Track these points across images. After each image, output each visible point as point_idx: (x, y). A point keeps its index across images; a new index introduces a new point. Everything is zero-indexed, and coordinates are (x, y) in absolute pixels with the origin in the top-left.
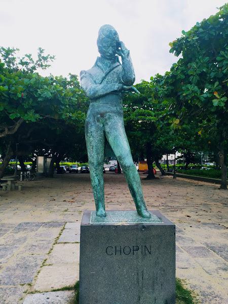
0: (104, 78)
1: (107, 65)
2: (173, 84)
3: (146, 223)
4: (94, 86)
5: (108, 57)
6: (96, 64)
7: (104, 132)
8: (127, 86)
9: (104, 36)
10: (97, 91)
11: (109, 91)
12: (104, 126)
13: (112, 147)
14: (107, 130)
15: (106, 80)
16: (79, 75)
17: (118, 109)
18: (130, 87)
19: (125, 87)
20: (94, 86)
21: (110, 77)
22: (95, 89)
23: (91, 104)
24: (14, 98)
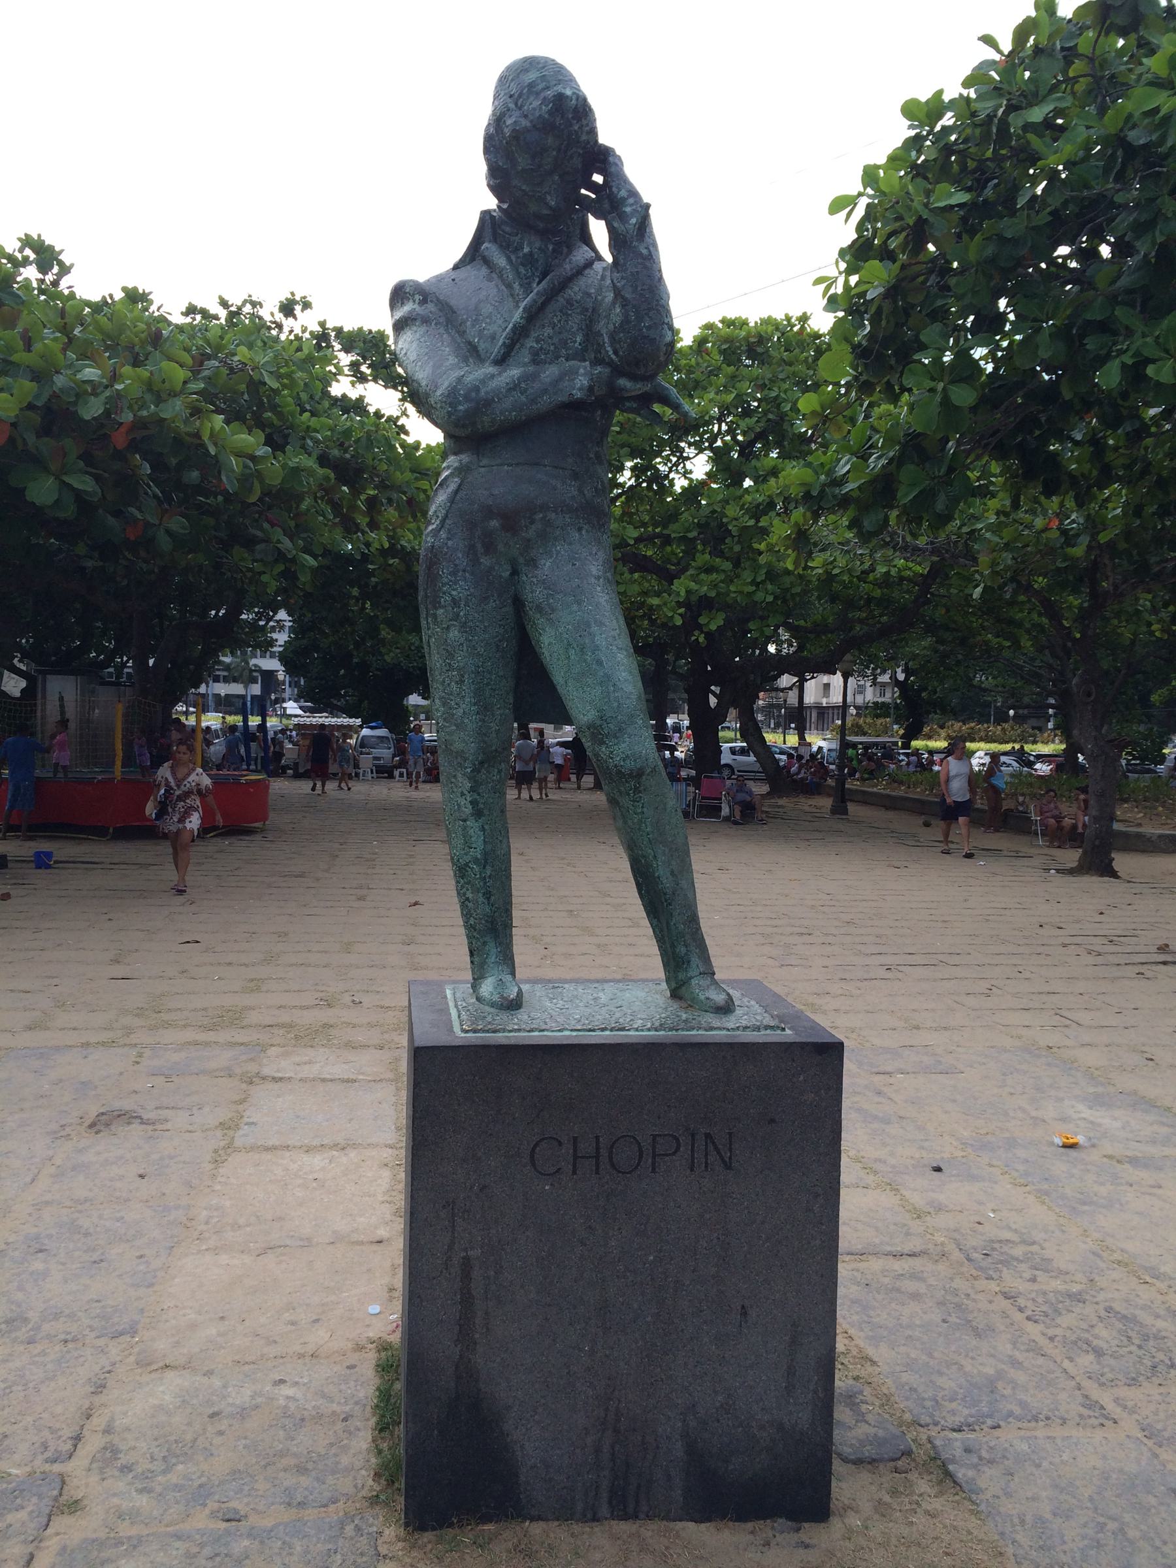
0: (519, 334)
1: (529, 260)
2: (749, 428)
3: (721, 1030)
4: (477, 373)
5: (541, 225)
6: (474, 253)
7: (518, 603)
8: (633, 377)
9: (525, 123)
10: (488, 403)
11: (546, 402)
12: (515, 572)
13: (558, 678)
14: (534, 594)
15: (530, 343)
16: (389, 332)
17: (588, 494)
18: (647, 387)
19: (623, 382)
20: (477, 373)
21: (548, 331)
22: (477, 389)
23: (8, 1340)
24: (686, 723)
